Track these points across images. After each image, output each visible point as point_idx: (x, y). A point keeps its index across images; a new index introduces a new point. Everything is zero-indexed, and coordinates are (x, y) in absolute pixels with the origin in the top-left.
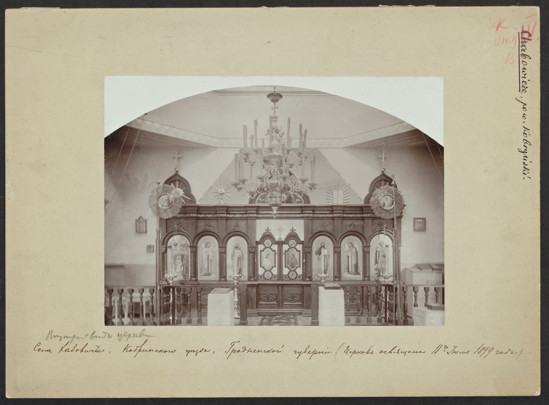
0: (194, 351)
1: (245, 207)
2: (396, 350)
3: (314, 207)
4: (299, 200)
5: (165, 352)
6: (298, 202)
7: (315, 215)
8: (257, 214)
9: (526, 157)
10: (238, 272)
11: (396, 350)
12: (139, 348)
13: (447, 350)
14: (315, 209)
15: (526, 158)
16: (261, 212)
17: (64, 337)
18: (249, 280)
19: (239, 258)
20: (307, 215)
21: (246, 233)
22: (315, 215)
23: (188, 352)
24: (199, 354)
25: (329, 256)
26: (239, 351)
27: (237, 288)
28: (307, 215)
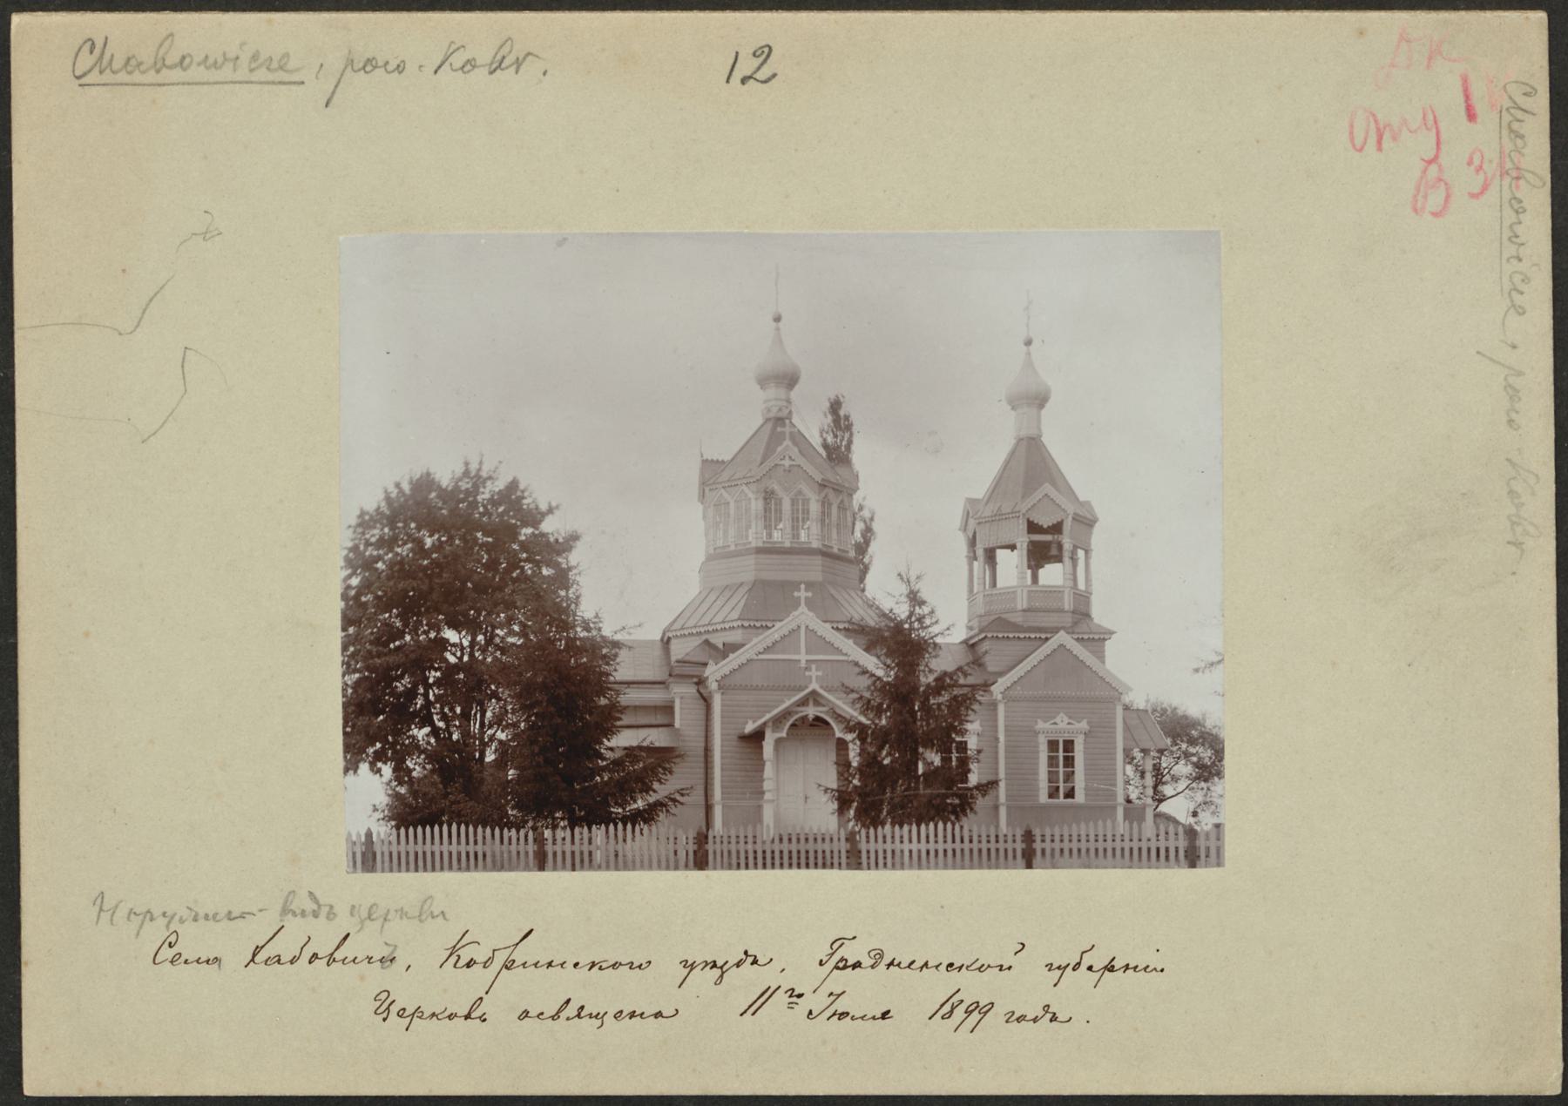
0: (714, 965)
2: (571, 1010)
5: (615, 966)
11: (571, 1010)
12: (500, 958)
13: (804, 1005)
23: (690, 966)
24: (732, 975)
26: (857, 965)
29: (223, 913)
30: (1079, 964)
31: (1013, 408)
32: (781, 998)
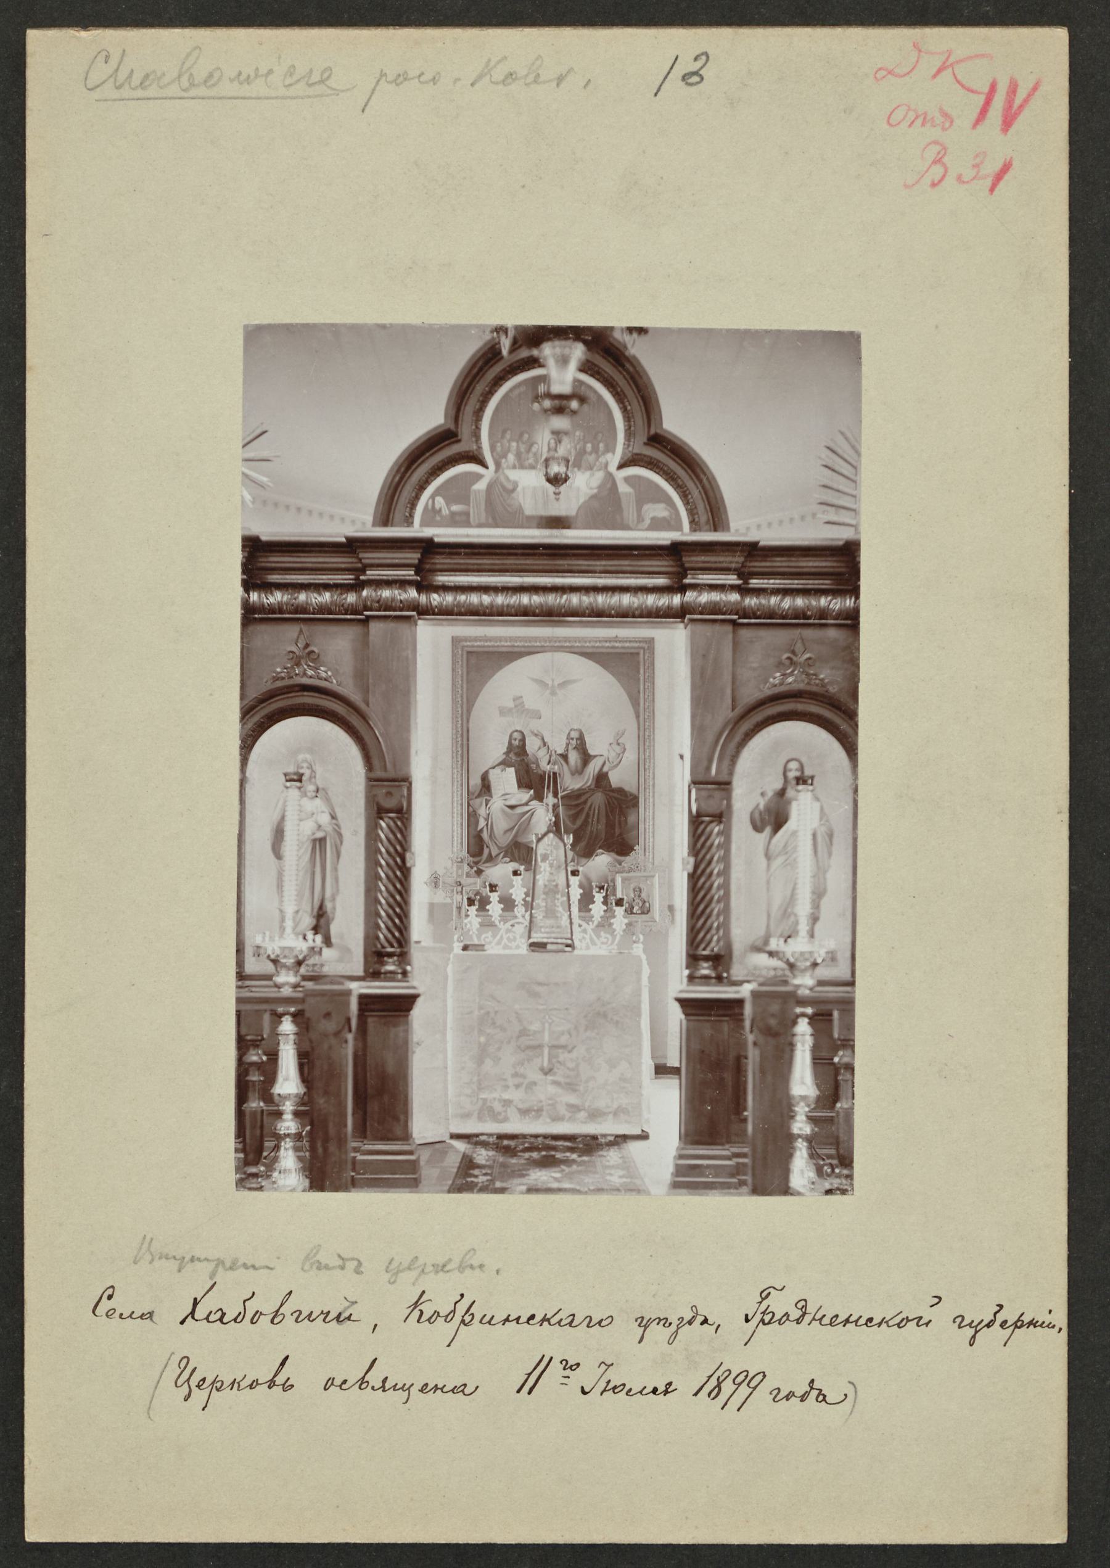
1: (353, 546)
3: (752, 549)
4: (659, 511)
6: (657, 524)
7: (751, 602)
8: (421, 587)
10: (308, 921)
14: (758, 565)
16: (442, 579)
17: (192, 1260)
18: (373, 974)
19: (319, 844)
20: (705, 598)
21: (355, 697)
22: (751, 602)
25: (831, 835)
27: (297, 1017)
28: (705, 598)
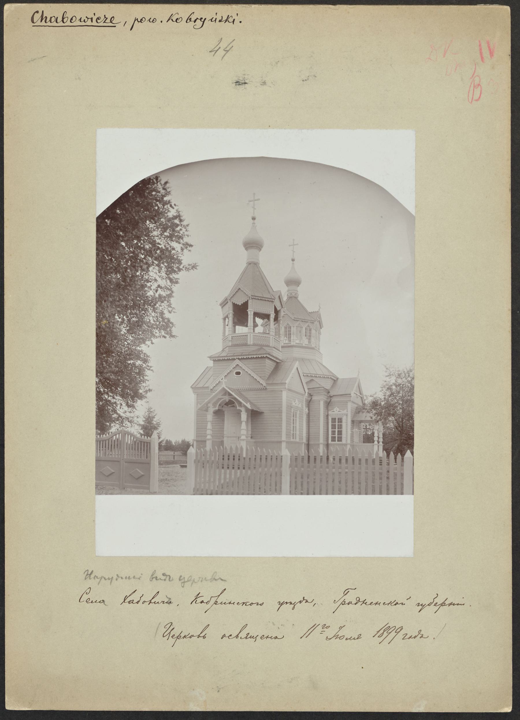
9: (80, 19)
12: (214, 600)
15: (214, 20)
23: (281, 604)
29: (132, 577)
30: (139, 601)
31: (246, 249)
32: (319, 628)
